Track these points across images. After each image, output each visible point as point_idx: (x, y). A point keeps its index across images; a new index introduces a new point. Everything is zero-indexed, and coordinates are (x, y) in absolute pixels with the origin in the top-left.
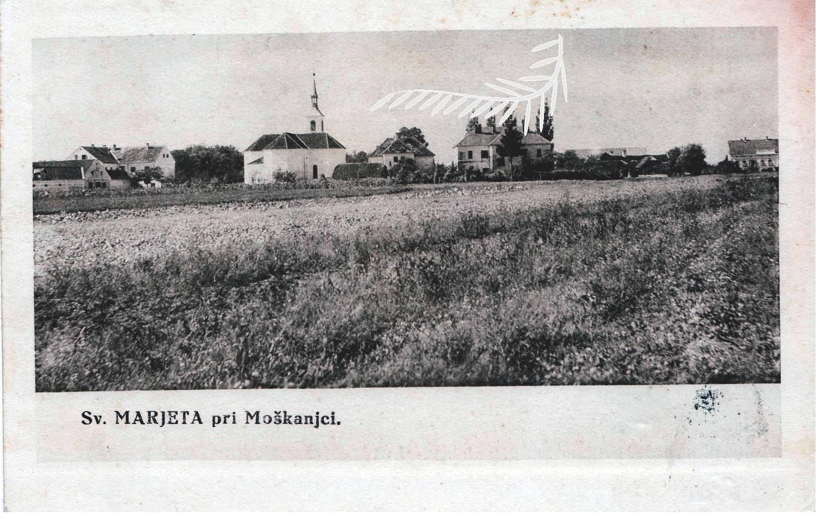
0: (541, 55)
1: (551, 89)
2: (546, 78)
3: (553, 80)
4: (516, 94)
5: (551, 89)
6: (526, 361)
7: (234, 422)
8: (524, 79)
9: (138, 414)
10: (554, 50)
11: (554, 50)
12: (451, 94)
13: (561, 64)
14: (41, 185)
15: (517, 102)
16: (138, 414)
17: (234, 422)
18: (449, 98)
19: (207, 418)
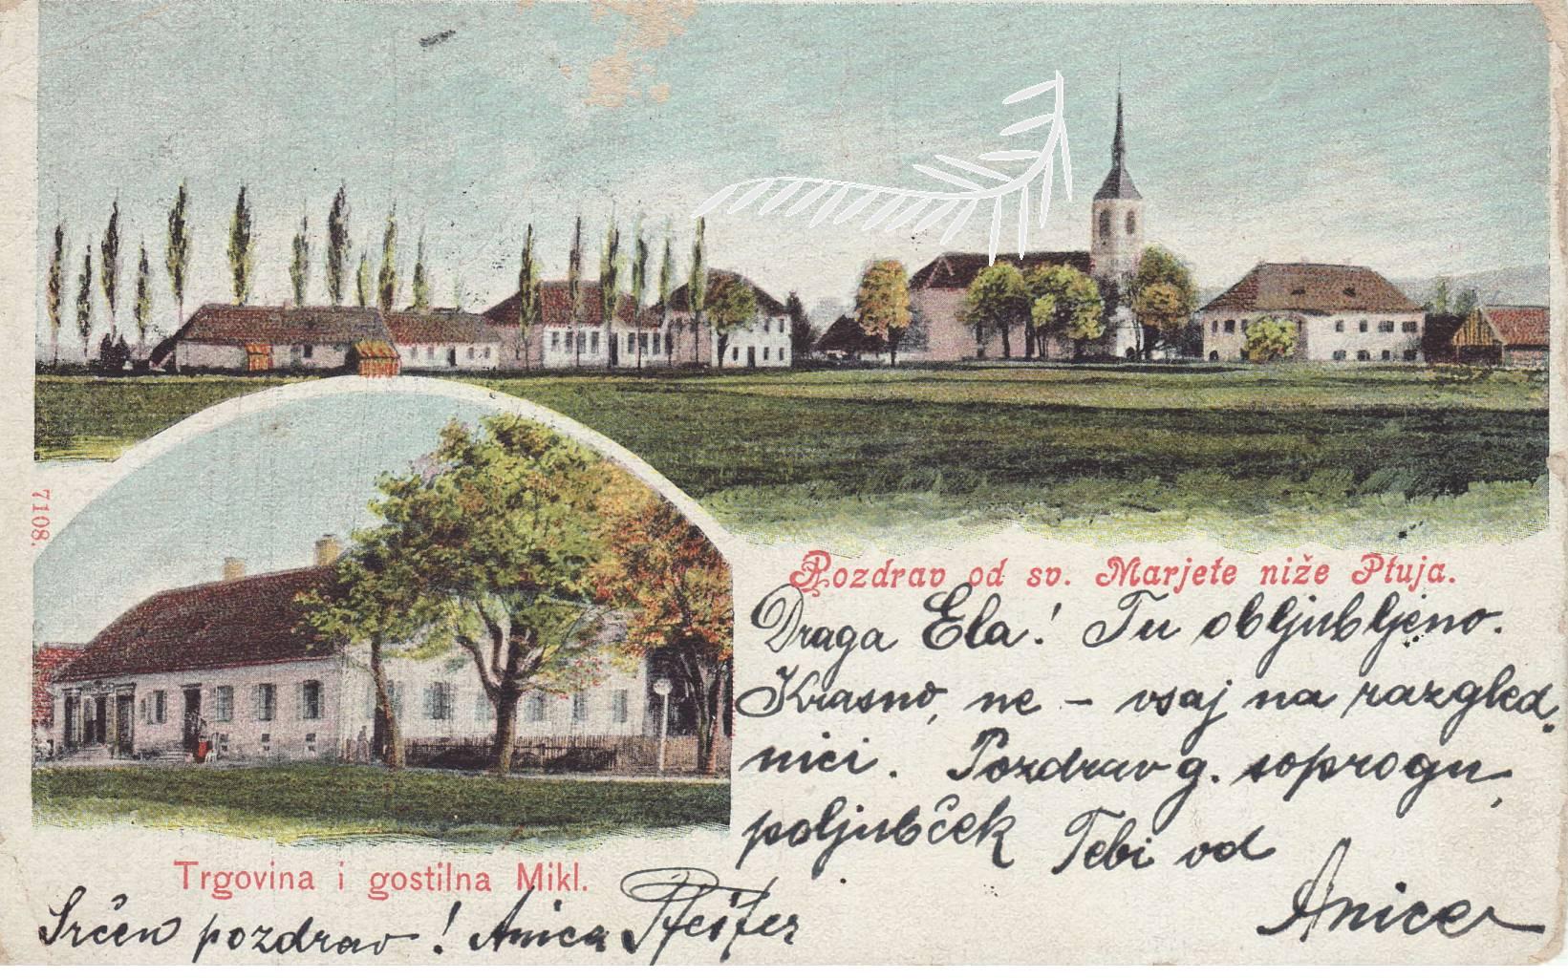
0: (1015, 141)
1: (1041, 174)
2: (1035, 154)
3: (1044, 159)
4: (973, 185)
5: (1041, 174)
6: (1044, 963)
7: (1303, 938)
8: (983, 157)
9: (260, 885)
10: (1045, 102)
11: (1045, 102)
12: (848, 185)
13: (1059, 131)
14: (725, 781)
15: (976, 200)
16: (260, 885)
17: (1303, 938)
18: (839, 196)
19: (613, 942)
